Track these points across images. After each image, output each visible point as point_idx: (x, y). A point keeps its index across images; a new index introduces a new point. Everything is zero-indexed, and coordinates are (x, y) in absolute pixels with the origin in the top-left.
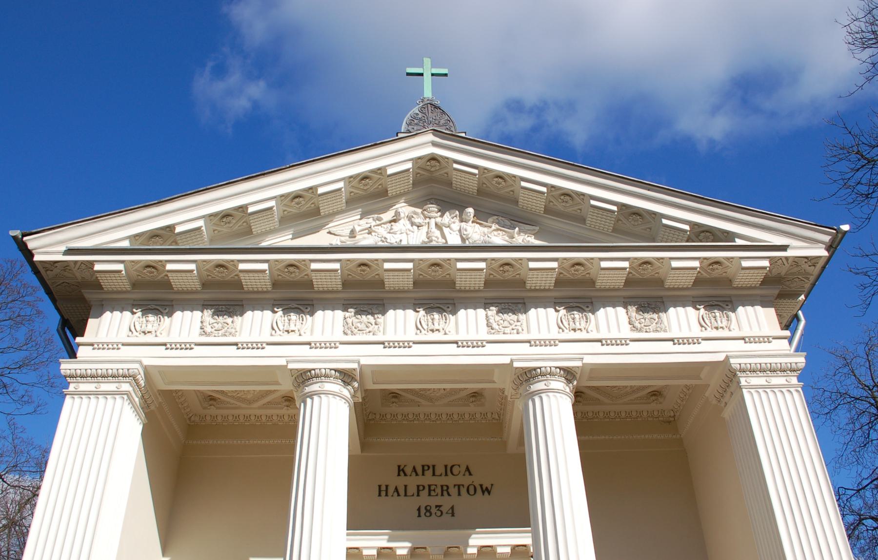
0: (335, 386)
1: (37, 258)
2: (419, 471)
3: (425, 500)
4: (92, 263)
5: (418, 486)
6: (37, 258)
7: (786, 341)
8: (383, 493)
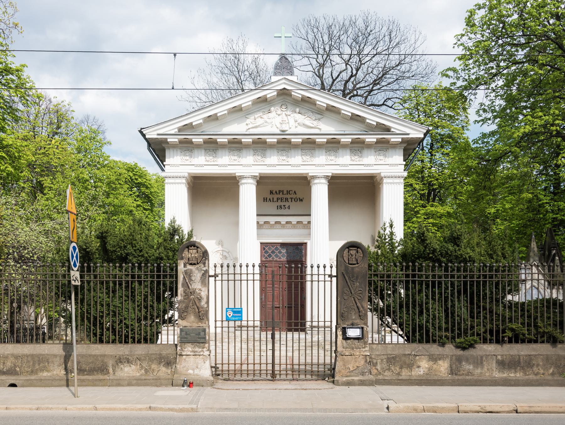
0: (251, 181)
1: (147, 137)
2: (278, 192)
3: (279, 203)
6: (147, 137)
7: (330, 274)
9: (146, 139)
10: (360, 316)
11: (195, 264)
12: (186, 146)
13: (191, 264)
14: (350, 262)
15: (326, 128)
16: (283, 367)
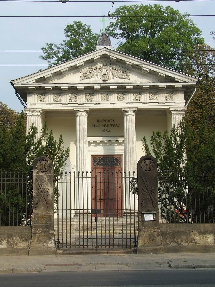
0: (84, 114)
1: (15, 86)
2: (102, 121)
3: (103, 128)
4: (28, 87)
5: (102, 125)
6: (15, 86)
8: (94, 127)
9: (14, 87)
10: (153, 205)
11: (44, 172)
12: (42, 91)
13: (42, 172)
14: (146, 169)
15: (134, 79)
16: (103, 241)
